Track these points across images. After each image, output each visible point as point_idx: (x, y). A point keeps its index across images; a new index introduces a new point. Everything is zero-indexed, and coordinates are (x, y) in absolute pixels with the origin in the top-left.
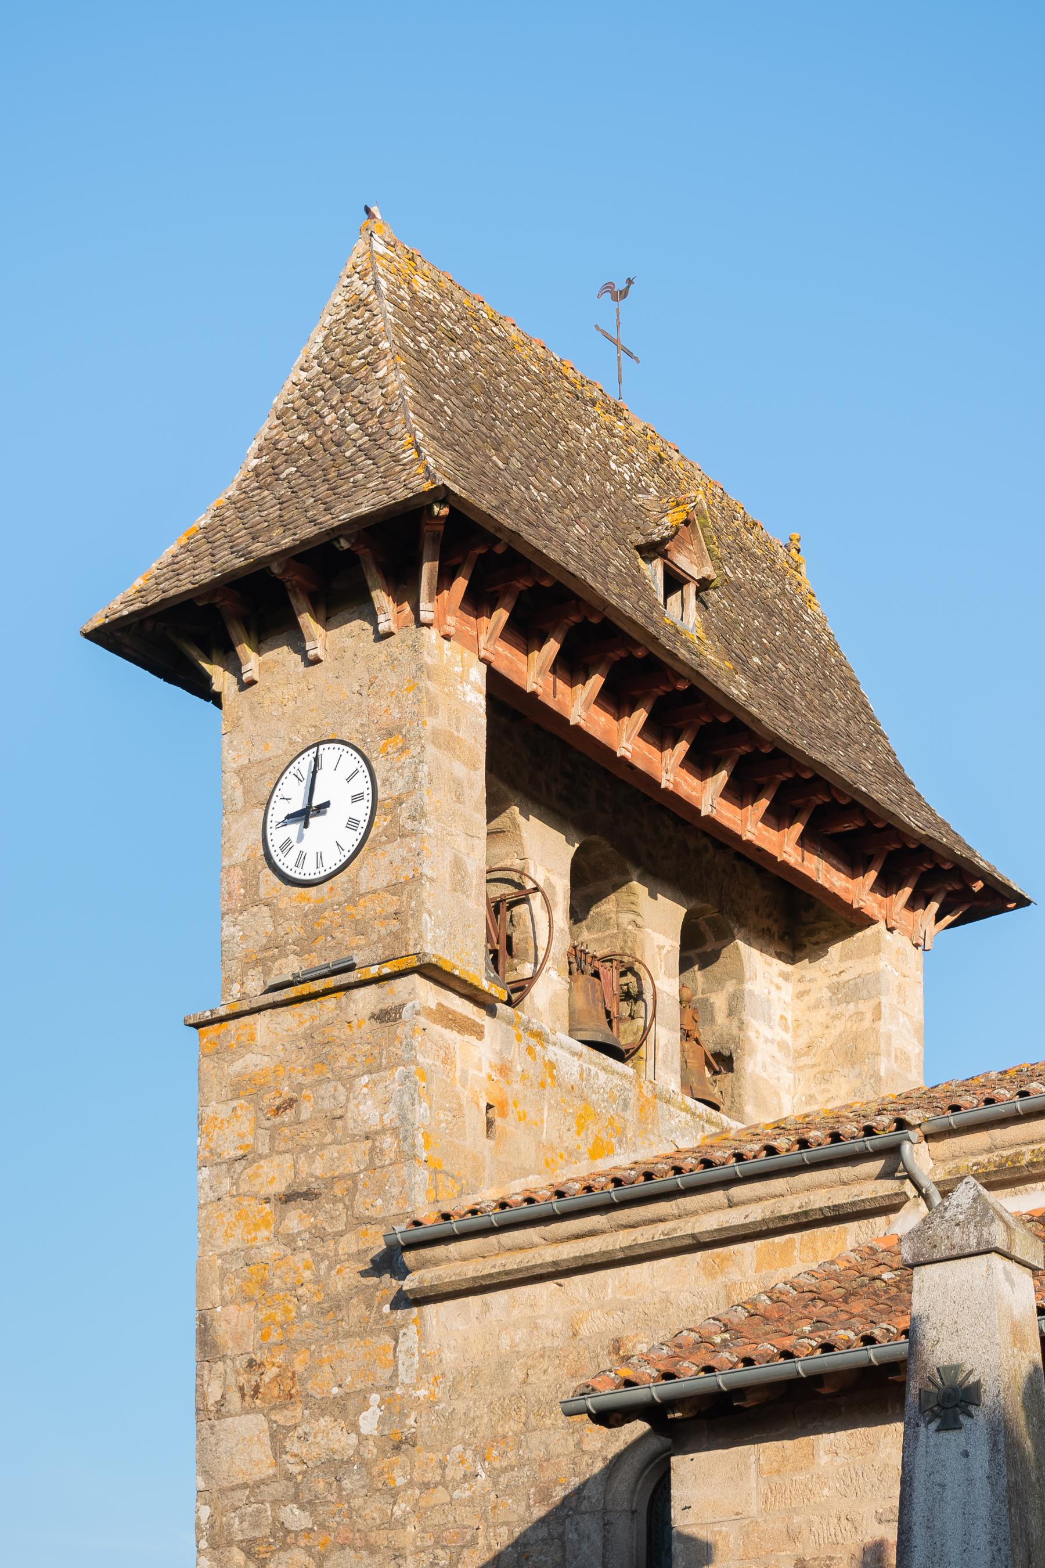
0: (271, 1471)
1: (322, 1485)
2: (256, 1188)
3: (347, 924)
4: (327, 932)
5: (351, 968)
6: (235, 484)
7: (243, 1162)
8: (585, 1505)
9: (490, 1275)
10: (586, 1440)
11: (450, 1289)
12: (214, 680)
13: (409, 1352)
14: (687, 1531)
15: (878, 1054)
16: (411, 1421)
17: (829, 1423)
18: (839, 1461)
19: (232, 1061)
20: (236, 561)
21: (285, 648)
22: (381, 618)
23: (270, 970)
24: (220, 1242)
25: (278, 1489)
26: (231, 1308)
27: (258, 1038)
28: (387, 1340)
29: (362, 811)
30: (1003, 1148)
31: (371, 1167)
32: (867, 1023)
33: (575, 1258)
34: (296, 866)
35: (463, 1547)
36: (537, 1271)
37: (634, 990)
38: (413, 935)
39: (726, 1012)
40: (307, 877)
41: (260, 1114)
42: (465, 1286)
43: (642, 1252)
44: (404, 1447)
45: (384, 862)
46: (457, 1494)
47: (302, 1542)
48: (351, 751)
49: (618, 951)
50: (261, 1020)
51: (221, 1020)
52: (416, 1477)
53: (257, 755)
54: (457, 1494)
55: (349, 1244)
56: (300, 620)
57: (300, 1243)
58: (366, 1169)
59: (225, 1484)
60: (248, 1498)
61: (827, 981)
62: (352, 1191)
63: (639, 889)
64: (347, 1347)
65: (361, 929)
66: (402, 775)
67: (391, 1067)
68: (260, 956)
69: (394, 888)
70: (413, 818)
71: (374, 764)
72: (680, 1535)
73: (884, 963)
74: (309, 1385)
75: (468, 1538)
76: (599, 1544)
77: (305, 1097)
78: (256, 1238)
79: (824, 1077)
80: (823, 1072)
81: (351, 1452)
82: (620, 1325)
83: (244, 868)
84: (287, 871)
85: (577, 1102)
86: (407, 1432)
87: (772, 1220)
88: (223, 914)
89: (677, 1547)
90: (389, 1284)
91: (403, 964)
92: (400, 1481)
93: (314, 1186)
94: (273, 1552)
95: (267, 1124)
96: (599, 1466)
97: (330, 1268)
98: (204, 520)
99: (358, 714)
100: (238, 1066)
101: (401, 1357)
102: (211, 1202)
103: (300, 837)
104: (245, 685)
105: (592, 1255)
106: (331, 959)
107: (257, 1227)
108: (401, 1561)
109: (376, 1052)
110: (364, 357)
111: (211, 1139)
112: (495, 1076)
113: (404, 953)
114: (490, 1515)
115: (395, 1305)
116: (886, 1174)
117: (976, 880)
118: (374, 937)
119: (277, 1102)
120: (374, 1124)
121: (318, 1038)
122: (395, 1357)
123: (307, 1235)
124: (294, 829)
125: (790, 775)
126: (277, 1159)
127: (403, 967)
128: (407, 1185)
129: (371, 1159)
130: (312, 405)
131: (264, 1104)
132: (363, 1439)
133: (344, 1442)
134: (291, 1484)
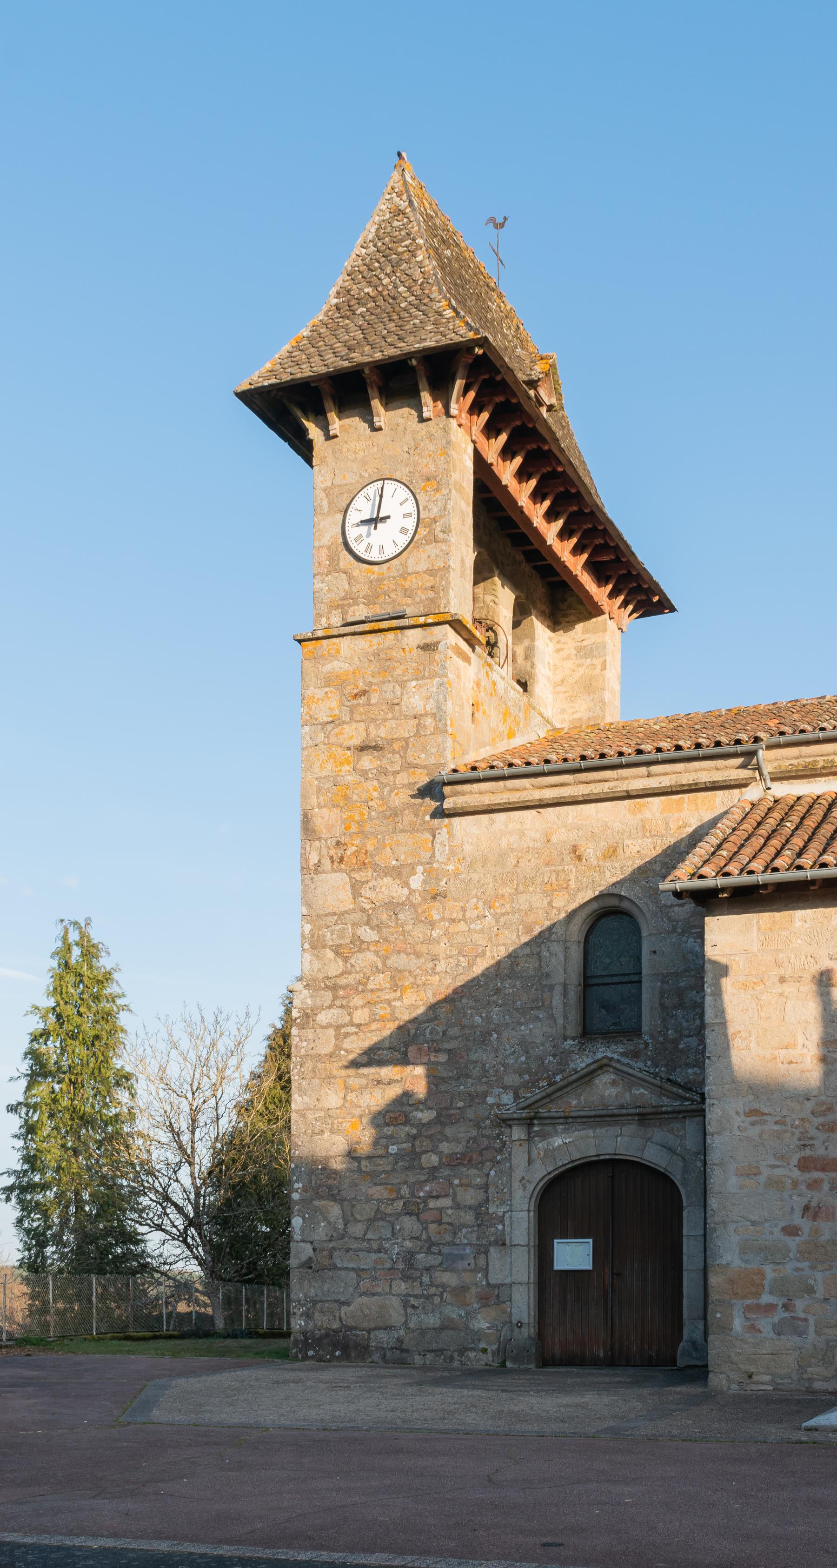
0: (352, 907)
1: (385, 916)
2: (341, 741)
3: (399, 590)
4: (386, 593)
5: (402, 617)
6: (323, 312)
7: (332, 725)
8: (554, 937)
9: (500, 804)
10: (555, 901)
11: (472, 810)
12: (310, 432)
13: (442, 844)
14: (714, 958)
15: (604, 689)
16: (443, 883)
17: (801, 905)
18: (807, 925)
19: (325, 664)
20: (341, 362)
21: (357, 418)
22: (425, 409)
23: (347, 612)
24: (317, 770)
25: (357, 917)
26: (325, 810)
27: (342, 652)
28: (428, 836)
29: (411, 524)
30: (805, 757)
31: (417, 735)
32: (598, 671)
33: (553, 798)
34: (366, 551)
35: (477, 956)
36: (528, 804)
37: (492, 641)
38: (443, 602)
39: (523, 657)
40: (373, 559)
41: (343, 697)
42: (482, 808)
43: (594, 797)
44: (438, 898)
45: (425, 556)
46: (472, 926)
47: (372, 948)
48: (403, 487)
49: (484, 617)
50: (345, 642)
51: (318, 639)
52: (447, 915)
53: (338, 481)
54: (472, 926)
55: (403, 778)
56: (372, 403)
57: (370, 776)
58: (414, 736)
59: (321, 912)
60: (336, 921)
61: (574, 645)
62: (406, 748)
63: (497, 580)
64: (401, 837)
65: (408, 593)
66: (436, 505)
67: (431, 677)
68: (340, 603)
69: (431, 572)
70: (444, 532)
71: (418, 496)
72: (710, 960)
73: (607, 638)
74: (377, 858)
75: (480, 951)
76: (563, 959)
77: (374, 690)
78: (341, 770)
79: (572, 699)
80: (571, 697)
81: (404, 899)
82: (576, 838)
83: (329, 548)
84: (360, 554)
85: (504, 706)
86: (440, 889)
87: (675, 786)
88: (315, 576)
89: (708, 966)
90: (431, 804)
91: (441, 618)
92: (436, 917)
93: (380, 743)
94: (353, 953)
95: (348, 704)
96: (563, 915)
97: (391, 792)
98: (306, 332)
99: (407, 465)
100: (328, 667)
101: (437, 846)
102: (311, 746)
103: (369, 535)
104: (329, 437)
105: (564, 797)
106: (389, 610)
107: (342, 764)
108: (436, 962)
109: (421, 668)
110: (407, 247)
111: (311, 709)
112: (475, 686)
113: (437, 611)
114: (494, 939)
115: (434, 816)
116: (743, 766)
117: (655, 595)
118: (417, 600)
119: (355, 691)
120: (420, 709)
121: (382, 656)
122: (433, 846)
123: (375, 771)
124: (364, 529)
125: (590, 526)
126: (354, 725)
127: (442, 620)
128: (441, 747)
129: (418, 731)
130: (372, 271)
131: (346, 692)
132: (412, 892)
133: (400, 893)
134: (364, 915)
